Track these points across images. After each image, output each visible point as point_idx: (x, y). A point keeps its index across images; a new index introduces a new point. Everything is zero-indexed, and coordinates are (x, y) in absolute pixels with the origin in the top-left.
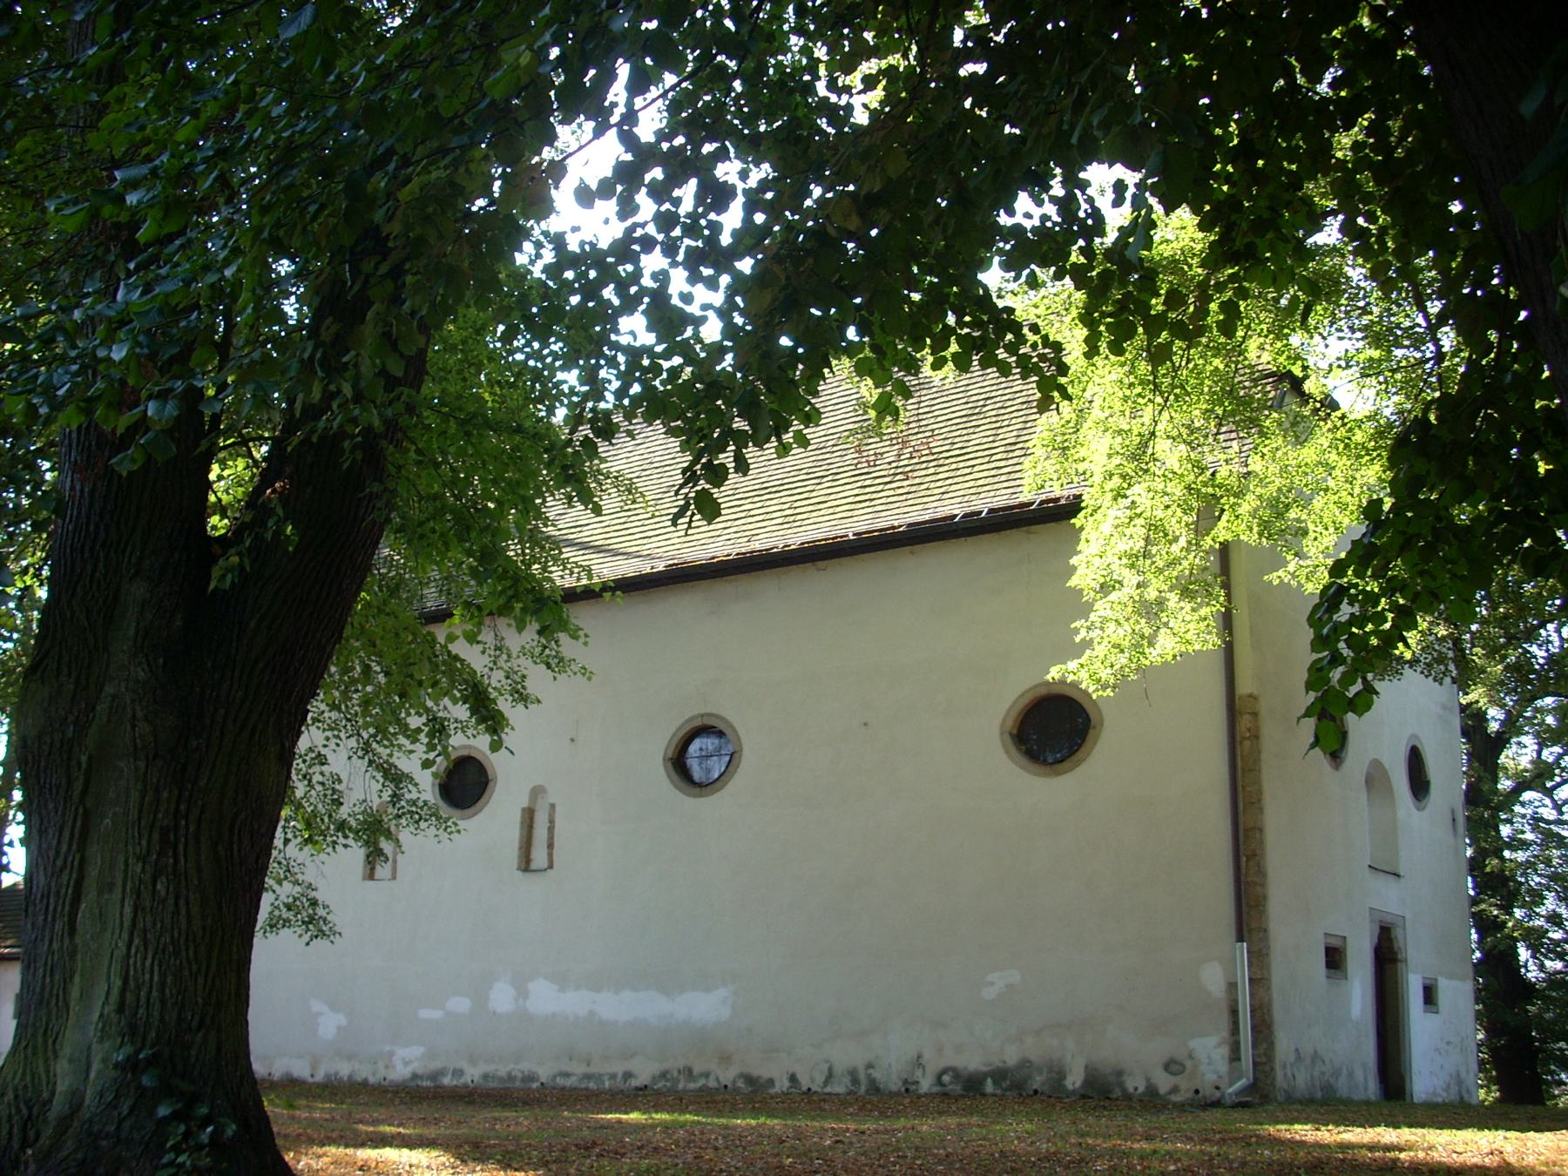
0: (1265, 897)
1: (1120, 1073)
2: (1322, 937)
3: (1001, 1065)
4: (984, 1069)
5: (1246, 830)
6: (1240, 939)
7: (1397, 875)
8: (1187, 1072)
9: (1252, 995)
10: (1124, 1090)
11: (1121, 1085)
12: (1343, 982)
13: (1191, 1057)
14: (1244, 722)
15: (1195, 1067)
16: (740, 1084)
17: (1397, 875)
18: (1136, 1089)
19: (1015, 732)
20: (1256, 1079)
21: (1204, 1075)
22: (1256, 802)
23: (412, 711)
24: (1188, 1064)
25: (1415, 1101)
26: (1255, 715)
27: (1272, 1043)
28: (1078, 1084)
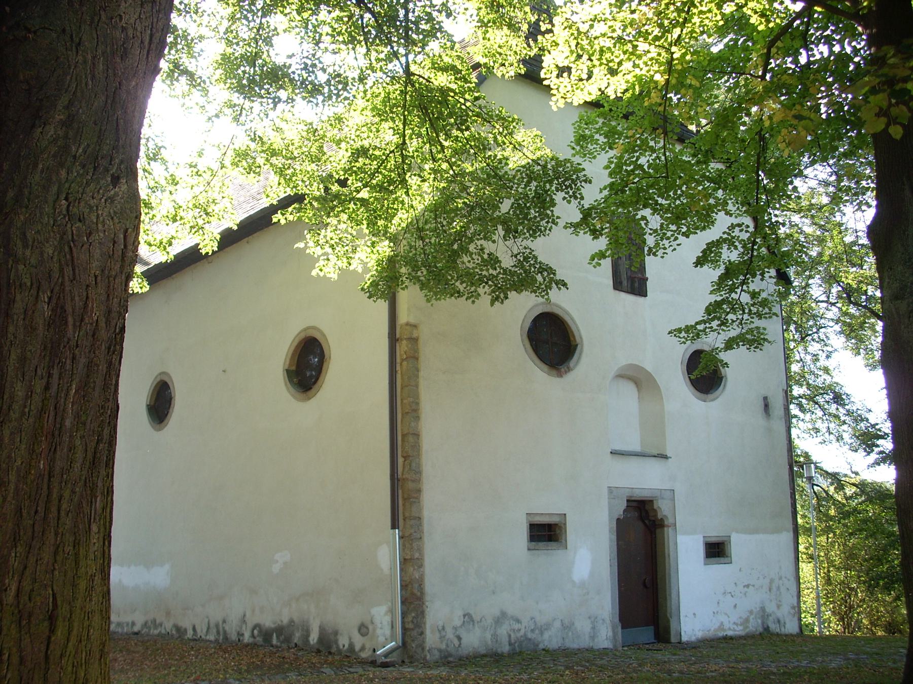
0: (419, 491)
1: (336, 633)
2: (525, 516)
3: (280, 623)
4: (273, 626)
5: (404, 436)
6: (394, 526)
7: (665, 457)
8: (369, 636)
9: (401, 570)
10: (338, 647)
11: (336, 642)
12: (560, 552)
13: (372, 623)
14: (402, 348)
15: (374, 630)
16: (174, 632)
17: (665, 457)
18: (344, 646)
19: (294, 368)
20: (404, 643)
21: (378, 636)
22: (414, 412)
23: (741, 344)
24: (371, 628)
25: (684, 638)
26: (414, 341)
27: (423, 613)
28: (315, 641)
